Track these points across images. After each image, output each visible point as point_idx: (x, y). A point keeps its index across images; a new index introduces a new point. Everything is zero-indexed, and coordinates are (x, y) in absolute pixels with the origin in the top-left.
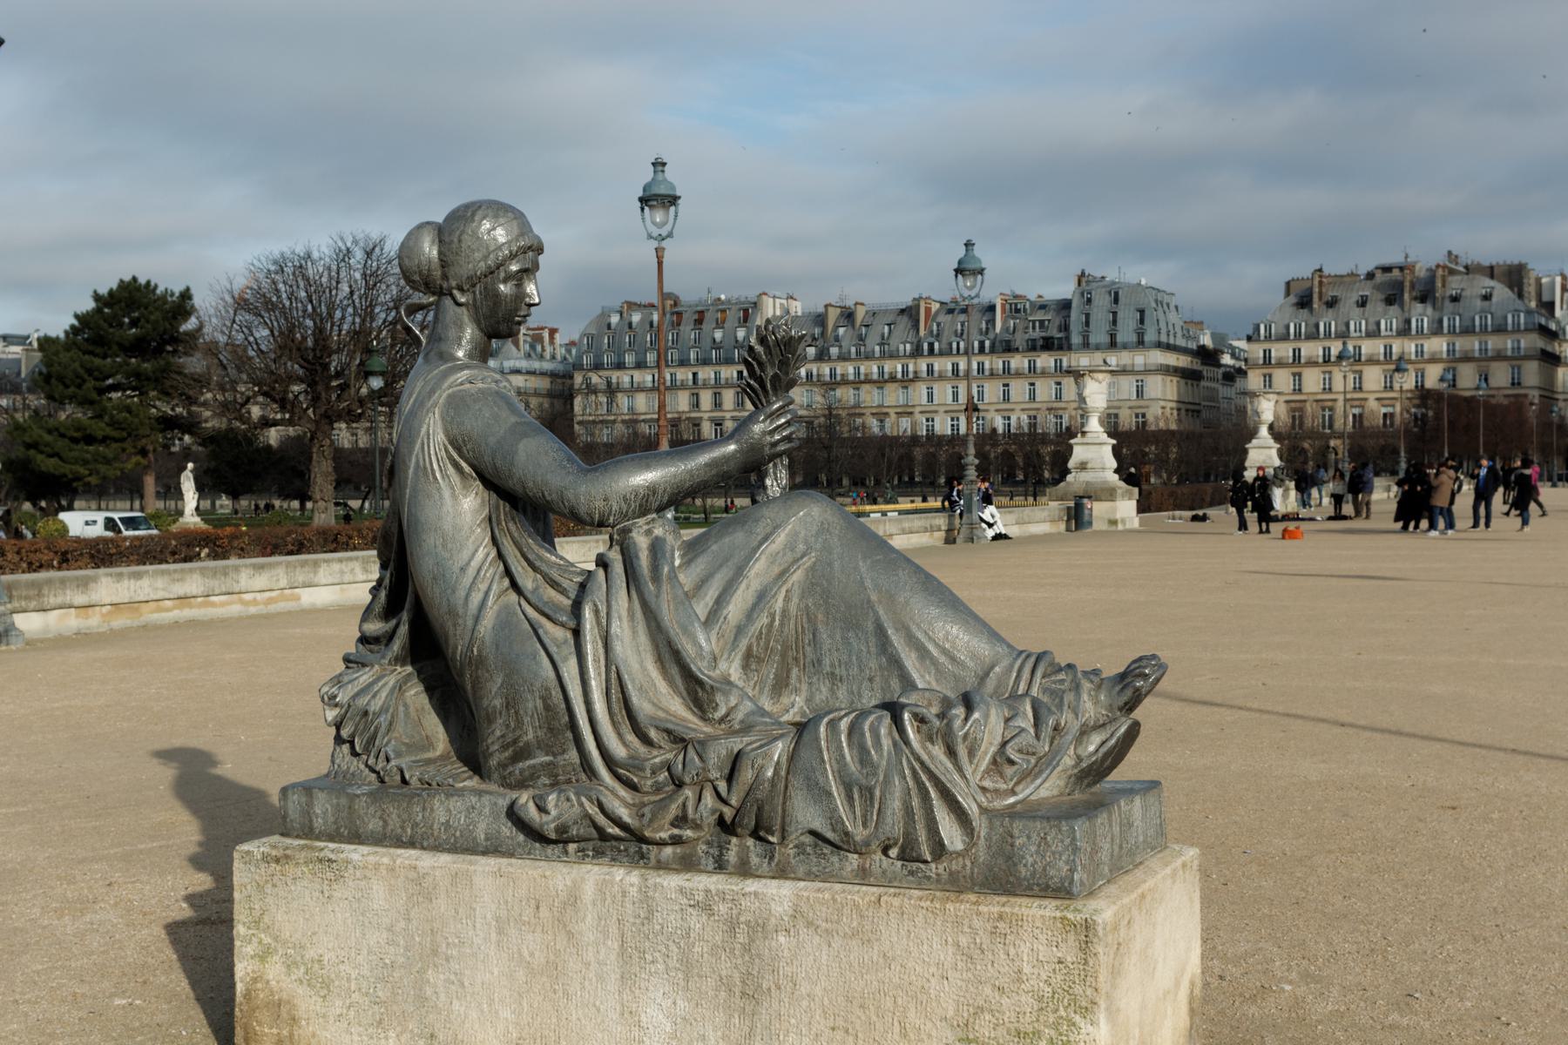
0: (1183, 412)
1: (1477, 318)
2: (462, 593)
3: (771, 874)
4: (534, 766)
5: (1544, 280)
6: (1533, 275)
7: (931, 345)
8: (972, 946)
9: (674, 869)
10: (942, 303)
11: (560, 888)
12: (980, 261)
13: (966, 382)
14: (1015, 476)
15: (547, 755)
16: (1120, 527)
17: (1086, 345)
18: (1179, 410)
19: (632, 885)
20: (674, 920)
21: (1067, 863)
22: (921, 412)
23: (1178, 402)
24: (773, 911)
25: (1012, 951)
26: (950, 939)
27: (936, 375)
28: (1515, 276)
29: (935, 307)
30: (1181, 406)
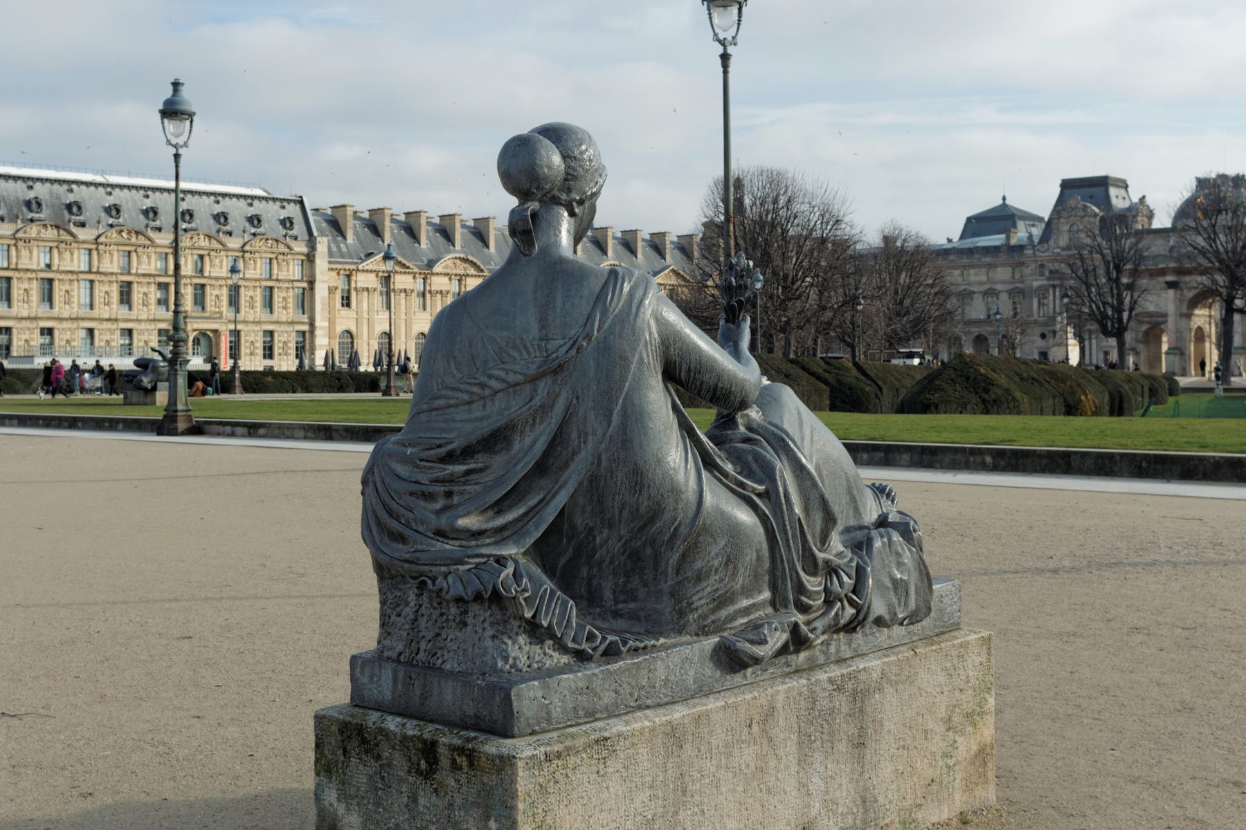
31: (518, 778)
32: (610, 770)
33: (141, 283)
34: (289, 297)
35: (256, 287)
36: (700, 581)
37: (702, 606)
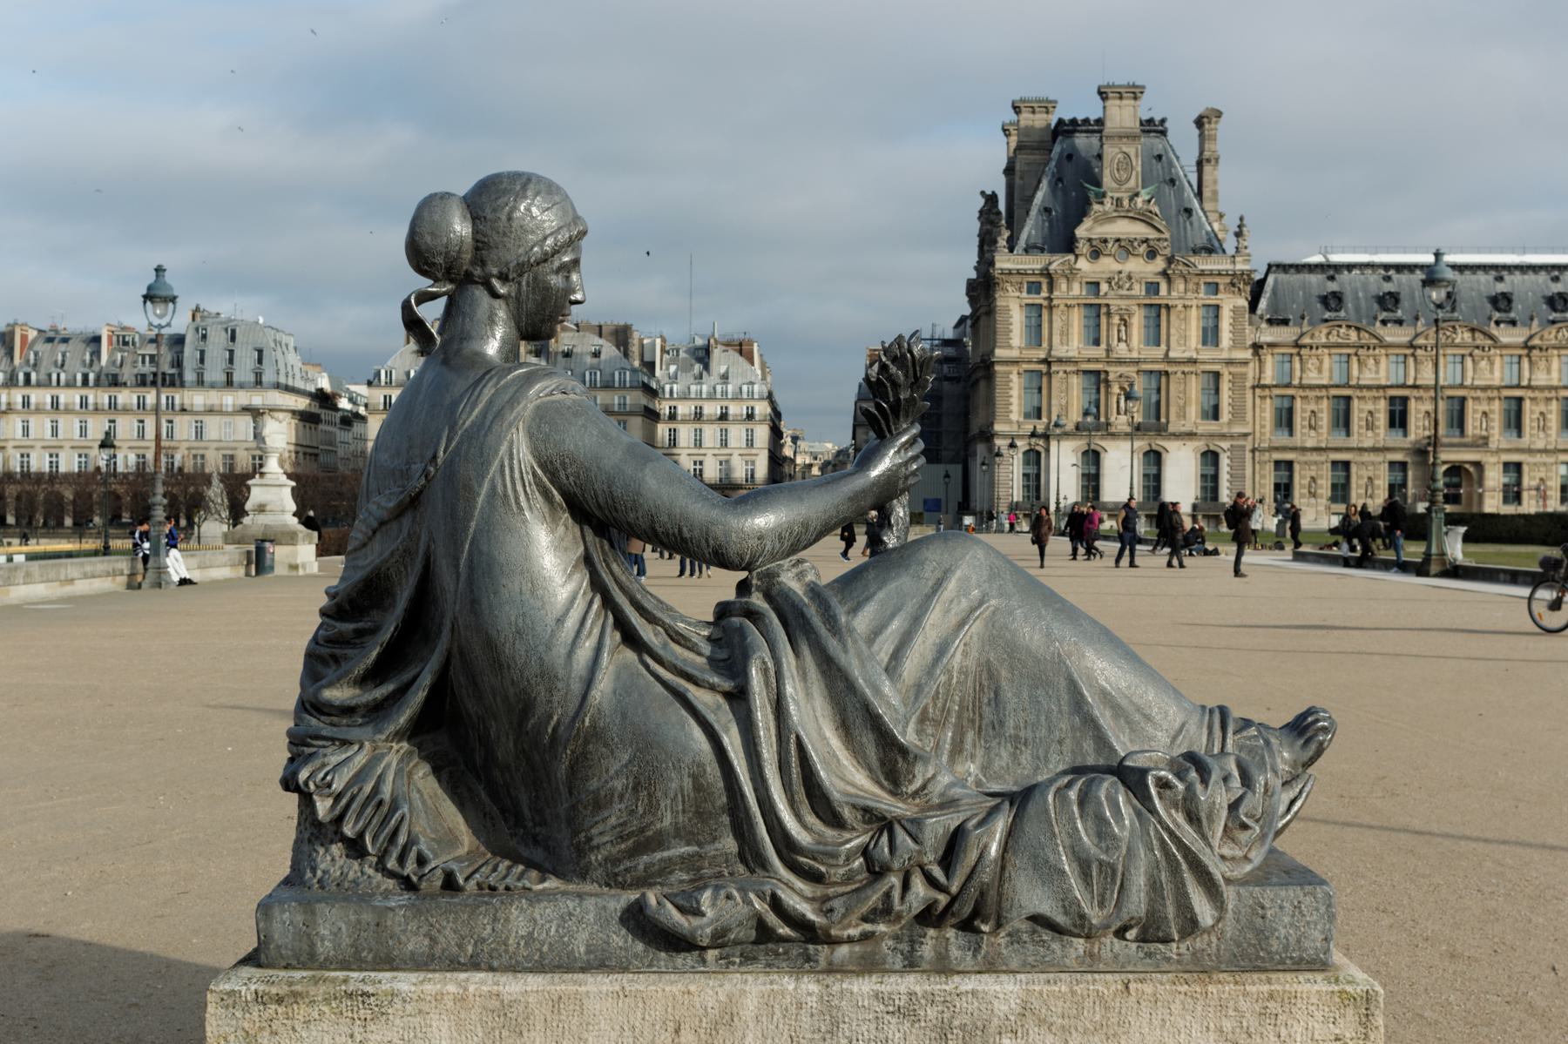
0: (301, 455)
1: (617, 374)
2: (560, 650)
3: (976, 968)
4: (670, 859)
5: (645, 341)
6: (636, 335)
7: (27, 377)
8: (1238, 1030)
9: (853, 972)
10: (40, 331)
11: (710, 1005)
12: (171, 288)
13: (154, 417)
14: (120, 517)
15: (688, 844)
16: (301, 572)
17: (200, 382)
18: (297, 453)
19: (809, 994)
20: (867, 1030)
21: (1322, 932)
22: (15, 447)
23: (296, 445)
24: (996, 1011)
25: (1284, 1032)
26: (1212, 1025)
27: (33, 407)
28: (621, 336)
29: (32, 334)
30: (299, 449)
31: (207, 1015)
33: (1307, 397)
34: (1379, 411)
35: (1322, 398)
36: (600, 808)
37: (604, 844)
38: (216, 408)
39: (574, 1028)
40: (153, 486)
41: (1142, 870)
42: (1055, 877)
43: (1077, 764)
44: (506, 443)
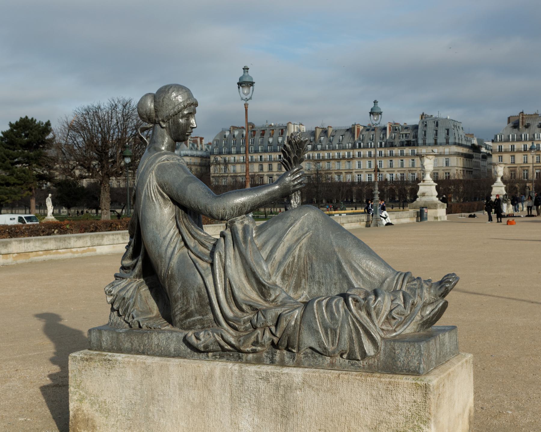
0: (465, 172)
2: (164, 248)
3: (293, 365)
4: (194, 320)
7: (360, 144)
8: (378, 395)
9: (254, 364)
10: (364, 127)
11: (205, 371)
13: (374, 159)
14: (395, 199)
15: (200, 316)
16: (439, 220)
17: (424, 144)
18: (463, 171)
19: (235, 370)
22: (356, 172)
23: (463, 168)
24: (294, 381)
25: (395, 397)
26: (368, 392)
27: (362, 156)
29: (361, 128)
30: (465, 169)
32: (111, 374)
38: (442, 154)
39: (166, 376)
40: (374, 187)
41: (346, 332)
42: (316, 333)
43: (342, 293)
44: (149, 179)
